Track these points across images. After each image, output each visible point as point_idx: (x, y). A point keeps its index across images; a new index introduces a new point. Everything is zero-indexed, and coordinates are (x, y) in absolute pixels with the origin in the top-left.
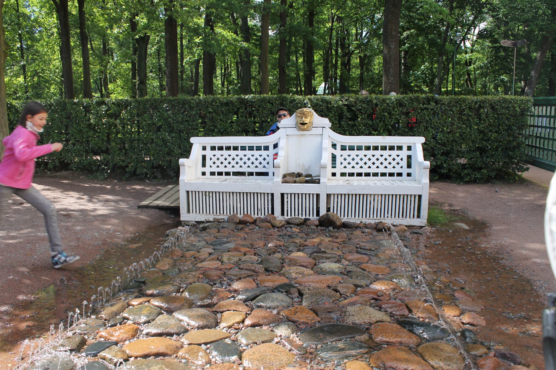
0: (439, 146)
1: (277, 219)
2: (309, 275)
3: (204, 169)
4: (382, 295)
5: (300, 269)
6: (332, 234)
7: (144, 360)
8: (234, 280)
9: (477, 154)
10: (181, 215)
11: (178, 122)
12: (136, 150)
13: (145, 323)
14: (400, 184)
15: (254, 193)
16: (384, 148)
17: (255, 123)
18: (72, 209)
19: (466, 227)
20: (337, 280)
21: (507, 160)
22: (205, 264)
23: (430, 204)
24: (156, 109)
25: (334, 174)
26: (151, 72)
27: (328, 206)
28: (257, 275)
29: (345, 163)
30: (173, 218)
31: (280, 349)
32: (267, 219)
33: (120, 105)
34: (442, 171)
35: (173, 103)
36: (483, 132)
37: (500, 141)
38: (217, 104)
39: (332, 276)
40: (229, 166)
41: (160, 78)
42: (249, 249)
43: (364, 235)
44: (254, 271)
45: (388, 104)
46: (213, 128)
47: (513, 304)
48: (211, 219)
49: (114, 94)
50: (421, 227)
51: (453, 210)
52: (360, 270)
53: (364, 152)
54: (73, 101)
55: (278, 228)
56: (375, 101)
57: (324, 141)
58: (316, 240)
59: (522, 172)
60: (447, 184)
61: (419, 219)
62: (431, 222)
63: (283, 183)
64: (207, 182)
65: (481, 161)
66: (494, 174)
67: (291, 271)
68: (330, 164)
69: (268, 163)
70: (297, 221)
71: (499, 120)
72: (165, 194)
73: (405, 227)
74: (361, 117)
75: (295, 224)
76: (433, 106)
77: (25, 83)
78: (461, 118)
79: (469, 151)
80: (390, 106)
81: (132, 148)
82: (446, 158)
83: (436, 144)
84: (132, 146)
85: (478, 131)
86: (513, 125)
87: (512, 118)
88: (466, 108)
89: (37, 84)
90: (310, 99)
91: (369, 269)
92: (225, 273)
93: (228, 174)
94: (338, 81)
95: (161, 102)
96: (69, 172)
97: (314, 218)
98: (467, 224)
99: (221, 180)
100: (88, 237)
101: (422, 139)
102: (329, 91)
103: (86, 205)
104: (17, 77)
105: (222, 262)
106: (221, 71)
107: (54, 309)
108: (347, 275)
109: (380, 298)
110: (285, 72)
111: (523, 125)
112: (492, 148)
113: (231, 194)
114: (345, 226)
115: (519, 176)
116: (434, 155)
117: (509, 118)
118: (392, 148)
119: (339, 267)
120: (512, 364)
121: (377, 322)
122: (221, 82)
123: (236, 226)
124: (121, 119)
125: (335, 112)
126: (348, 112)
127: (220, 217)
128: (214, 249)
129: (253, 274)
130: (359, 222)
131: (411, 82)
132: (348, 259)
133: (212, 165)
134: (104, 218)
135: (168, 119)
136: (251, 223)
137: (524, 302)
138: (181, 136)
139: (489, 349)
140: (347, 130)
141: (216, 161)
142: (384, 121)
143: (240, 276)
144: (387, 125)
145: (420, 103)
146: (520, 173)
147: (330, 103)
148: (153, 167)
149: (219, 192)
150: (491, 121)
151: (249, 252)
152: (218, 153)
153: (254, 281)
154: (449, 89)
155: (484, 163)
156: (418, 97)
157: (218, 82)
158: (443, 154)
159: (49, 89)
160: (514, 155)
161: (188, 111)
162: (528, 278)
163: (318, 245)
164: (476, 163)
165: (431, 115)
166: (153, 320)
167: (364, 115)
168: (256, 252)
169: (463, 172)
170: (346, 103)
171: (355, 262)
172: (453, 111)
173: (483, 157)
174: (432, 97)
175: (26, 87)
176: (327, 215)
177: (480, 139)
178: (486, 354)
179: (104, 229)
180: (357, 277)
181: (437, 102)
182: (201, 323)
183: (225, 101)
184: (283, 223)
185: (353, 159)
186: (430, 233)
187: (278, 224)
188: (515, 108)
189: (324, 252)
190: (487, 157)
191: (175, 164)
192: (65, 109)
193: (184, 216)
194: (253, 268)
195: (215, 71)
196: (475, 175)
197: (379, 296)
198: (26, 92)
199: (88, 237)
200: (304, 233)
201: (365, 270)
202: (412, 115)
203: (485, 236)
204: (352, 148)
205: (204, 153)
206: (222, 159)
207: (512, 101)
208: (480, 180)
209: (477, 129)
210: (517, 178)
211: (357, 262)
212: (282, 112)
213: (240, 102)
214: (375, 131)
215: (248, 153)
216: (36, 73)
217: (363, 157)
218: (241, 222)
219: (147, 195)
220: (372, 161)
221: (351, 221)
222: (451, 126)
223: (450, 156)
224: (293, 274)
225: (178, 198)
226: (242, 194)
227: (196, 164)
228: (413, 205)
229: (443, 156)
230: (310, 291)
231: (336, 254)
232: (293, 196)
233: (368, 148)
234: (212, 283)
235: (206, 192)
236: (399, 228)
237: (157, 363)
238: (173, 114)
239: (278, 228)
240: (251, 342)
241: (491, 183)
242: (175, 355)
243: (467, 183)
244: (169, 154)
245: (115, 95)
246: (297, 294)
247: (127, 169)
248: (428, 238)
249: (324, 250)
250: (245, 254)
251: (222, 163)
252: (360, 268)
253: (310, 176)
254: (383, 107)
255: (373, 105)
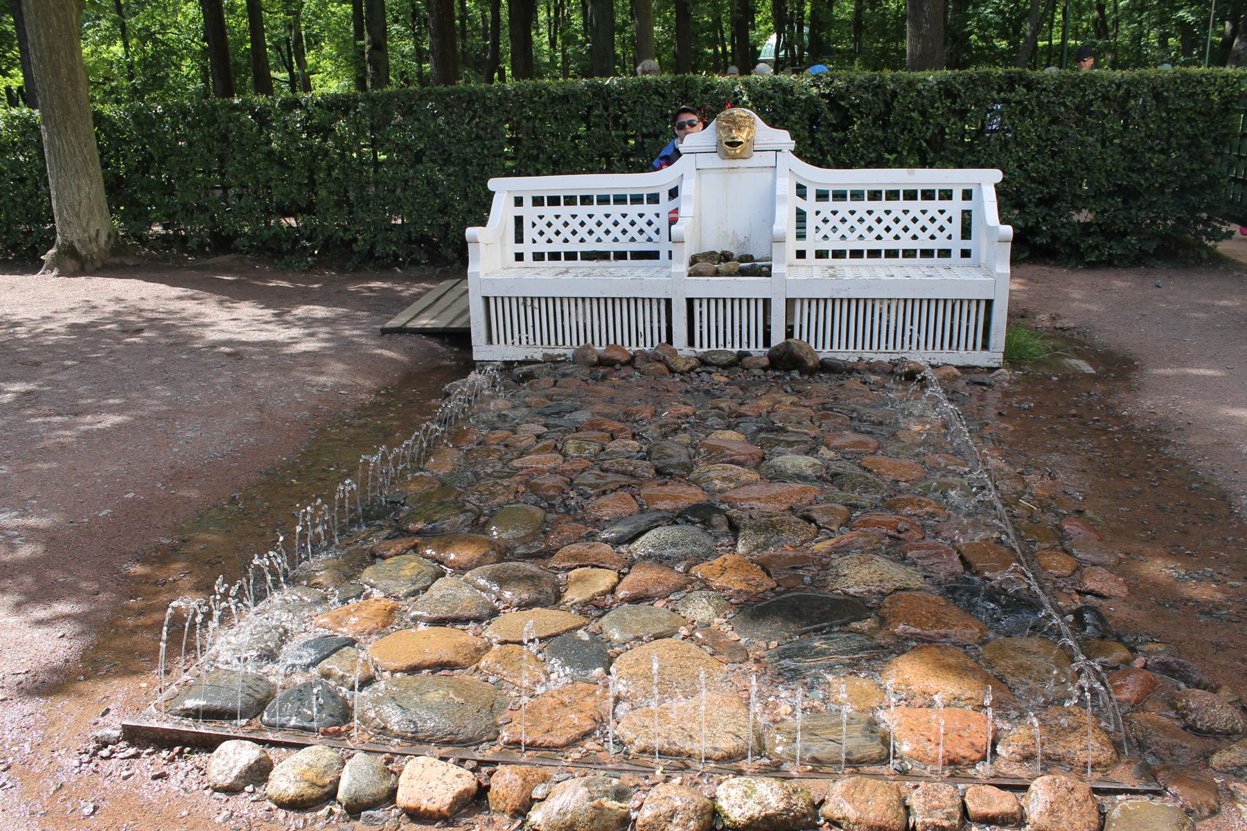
0: (1033, 186)
1: (679, 353)
2: (748, 484)
3: (519, 248)
4: (907, 530)
5: (731, 470)
6: (798, 387)
7: (410, 678)
8: (591, 495)
9: (1117, 202)
10: (474, 349)
11: (459, 141)
12: (371, 206)
13: (409, 595)
14: (946, 275)
15: (628, 299)
16: (910, 195)
17: (626, 138)
18: (244, 339)
19: (1088, 369)
20: (810, 496)
21: (1184, 215)
22: (530, 460)
23: (1010, 315)
24: (411, 114)
25: (801, 254)
26: (396, 21)
27: (789, 324)
28: (640, 485)
29: (825, 229)
30: (458, 352)
31: (692, 653)
32: (656, 354)
33: (336, 105)
34: (1038, 240)
35: (448, 99)
36: (1131, 151)
37: (1170, 172)
38: (543, 99)
39: (799, 486)
40: (574, 240)
41: (415, 35)
42: (620, 425)
43: (866, 388)
44: (632, 475)
45: (919, 92)
46: (535, 152)
47: (1188, 549)
48: (539, 357)
49: (319, 73)
50: (991, 370)
51: (1061, 328)
52: (859, 471)
53: (867, 204)
54: (231, 103)
55: (682, 373)
56: (891, 86)
57: (779, 182)
58: (765, 403)
59: (1216, 240)
60: (1047, 268)
61: (985, 352)
62: (1013, 357)
63: (690, 275)
64: (526, 277)
65: (1125, 218)
66: (1154, 245)
67: (712, 474)
68: (793, 232)
69: (657, 232)
70: (723, 358)
71: (1169, 124)
72: (437, 300)
73: (955, 370)
74: (859, 122)
75: (718, 366)
76: (1020, 96)
77: (127, 56)
78: (1083, 120)
79: (1098, 195)
80: (924, 97)
81: (364, 200)
82: (1045, 210)
83: (1025, 179)
84: (362, 197)
85: (1120, 150)
86: (1203, 135)
87: (1202, 118)
88: (1096, 99)
89: (153, 56)
90: (746, 84)
91: (879, 469)
92: (572, 481)
93: (571, 256)
94: (806, 30)
95: (420, 99)
96: (233, 256)
97: (758, 351)
98: (1090, 362)
99: (558, 271)
100: (282, 401)
101: (996, 175)
102: (786, 52)
103: (273, 331)
104: (109, 45)
105: (565, 455)
106: (549, 15)
107: (220, 562)
108: (832, 482)
109: (902, 536)
110: (689, 16)
111: (1226, 135)
112: (1151, 188)
113: (580, 302)
114: (826, 367)
115: (1210, 250)
116: (1020, 206)
117: (1194, 120)
118: (928, 195)
119: (814, 464)
120: (1182, 685)
121: (897, 590)
122: (550, 38)
123: (591, 372)
124: (335, 138)
125: (803, 112)
126: (831, 110)
127: (556, 352)
128: (546, 426)
129: (631, 482)
130: (856, 359)
131: (971, 33)
132: (832, 445)
133: (537, 238)
134: (314, 360)
135: (436, 135)
136: (623, 364)
137: (1213, 542)
138: (466, 170)
139: (1133, 650)
140: (828, 151)
141: (545, 229)
142: (910, 131)
143: (603, 489)
144: (918, 139)
145: (992, 88)
146: (1211, 244)
147: (791, 91)
148: (409, 241)
149: (554, 299)
150: (1152, 126)
151: (622, 430)
152: (548, 211)
153: (634, 497)
154: (1054, 42)
155: (1131, 222)
156: (988, 74)
157: (542, 38)
158: (1041, 202)
159: (178, 67)
160: (1200, 203)
161: (480, 117)
162: (1223, 487)
163: (768, 412)
164: (1113, 221)
165: (1016, 116)
166: (426, 589)
167: (867, 116)
168: (635, 431)
169: (1084, 241)
170: (827, 92)
171: (847, 453)
172: (1066, 106)
173: (1131, 208)
174: (1019, 73)
175: (130, 66)
176: (787, 344)
177: (1124, 169)
178: (1127, 662)
179: (313, 383)
180: (853, 488)
181: (1029, 86)
182: (525, 596)
183: (560, 92)
184: (693, 362)
185: (599, 224)
186: (1009, 382)
187: (681, 365)
188: (1209, 95)
189: (782, 430)
190: (1140, 208)
191: (456, 234)
192: (215, 121)
193: (481, 351)
194: (632, 468)
195: (534, 15)
196: (1110, 248)
197: (900, 532)
198: (131, 78)
199: (282, 401)
200: (738, 384)
201: (870, 471)
202: (972, 116)
203: (1129, 389)
204: (840, 196)
205: (519, 211)
206: (558, 224)
207: (1204, 79)
208: (1121, 260)
209: (1120, 145)
210: (1204, 255)
211: (852, 452)
212: (686, 117)
213: (594, 94)
214: (890, 153)
215: (615, 210)
216: (147, 35)
217: (866, 216)
218: (604, 362)
219: (402, 303)
220: (883, 225)
221: (840, 357)
222: (1060, 140)
223: (1055, 206)
224: (717, 482)
225: (467, 310)
226: (602, 302)
227: (503, 239)
228: (972, 322)
229: (1041, 208)
230: (753, 522)
231: (806, 434)
232: (713, 303)
233: (875, 195)
234: (544, 504)
235: (525, 298)
236: (943, 372)
237: (438, 685)
238: (448, 123)
239: (682, 373)
240: (631, 636)
241: (1146, 266)
242: (474, 667)
243: (1092, 266)
244: (443, 211)
245: (321, 75)
246: (725, 528)
247: (354, 245)
248: (1006, 394)
249: (780, 425)
250: (613, 438)
251: (558, 233)
252: (860, 466)
253: (749, 258)
254: (908, 99)
255: (885, 95)
